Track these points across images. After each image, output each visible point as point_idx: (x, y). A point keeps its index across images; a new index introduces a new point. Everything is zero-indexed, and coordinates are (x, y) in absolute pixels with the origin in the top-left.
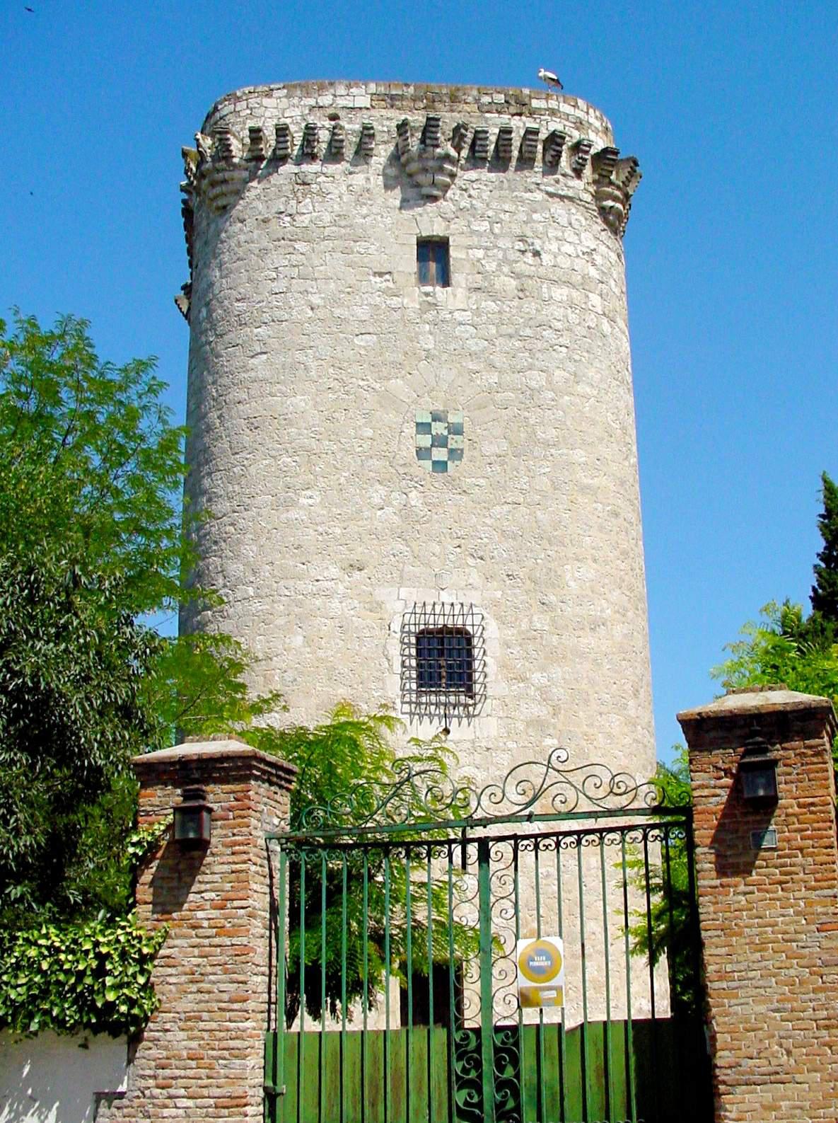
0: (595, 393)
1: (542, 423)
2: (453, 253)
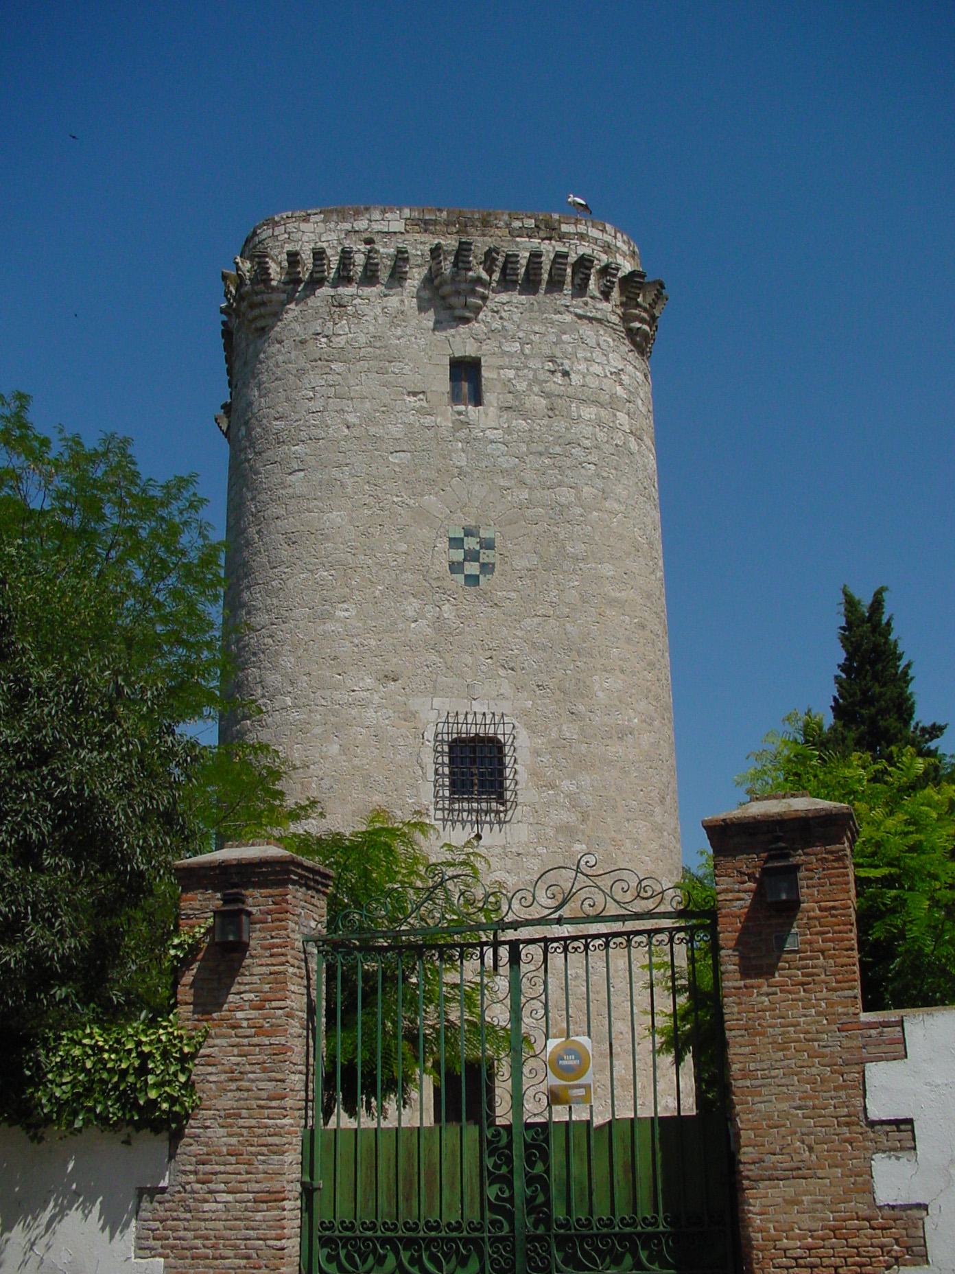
0: (623, 508)
1: (570, 539)
2: (485, 373)
